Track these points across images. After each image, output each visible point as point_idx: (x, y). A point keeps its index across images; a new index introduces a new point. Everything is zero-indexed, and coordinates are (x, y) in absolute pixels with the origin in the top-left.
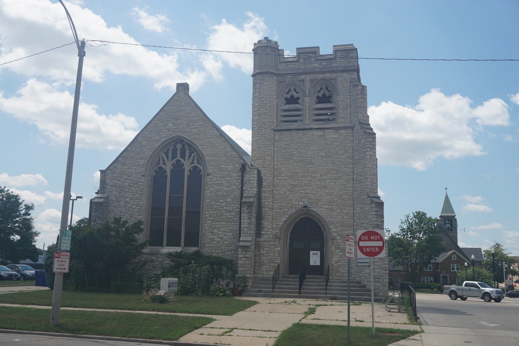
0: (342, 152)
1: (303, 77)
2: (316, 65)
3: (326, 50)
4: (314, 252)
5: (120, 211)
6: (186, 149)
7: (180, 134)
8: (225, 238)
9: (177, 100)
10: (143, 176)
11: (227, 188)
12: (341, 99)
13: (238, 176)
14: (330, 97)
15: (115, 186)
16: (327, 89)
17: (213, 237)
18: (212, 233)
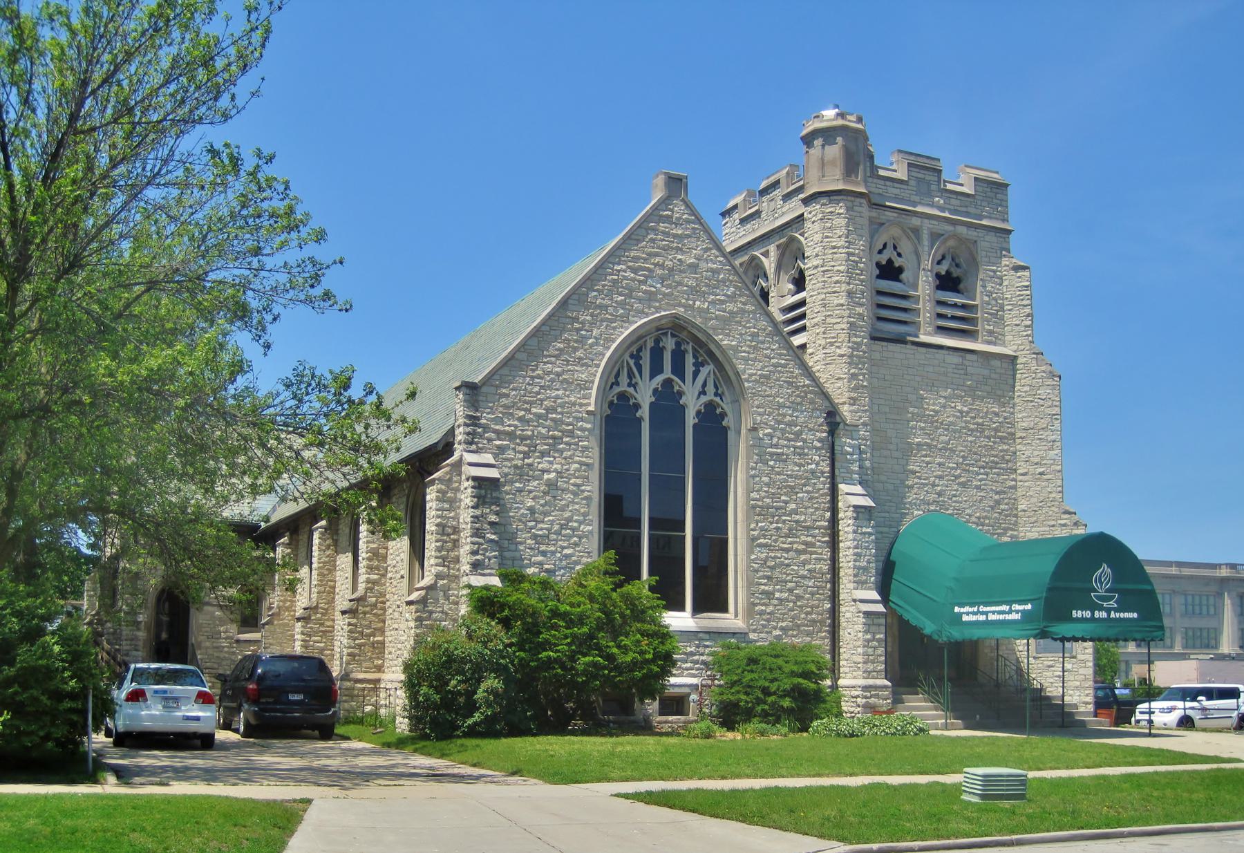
6: (685, 351)
16: (895, 248)
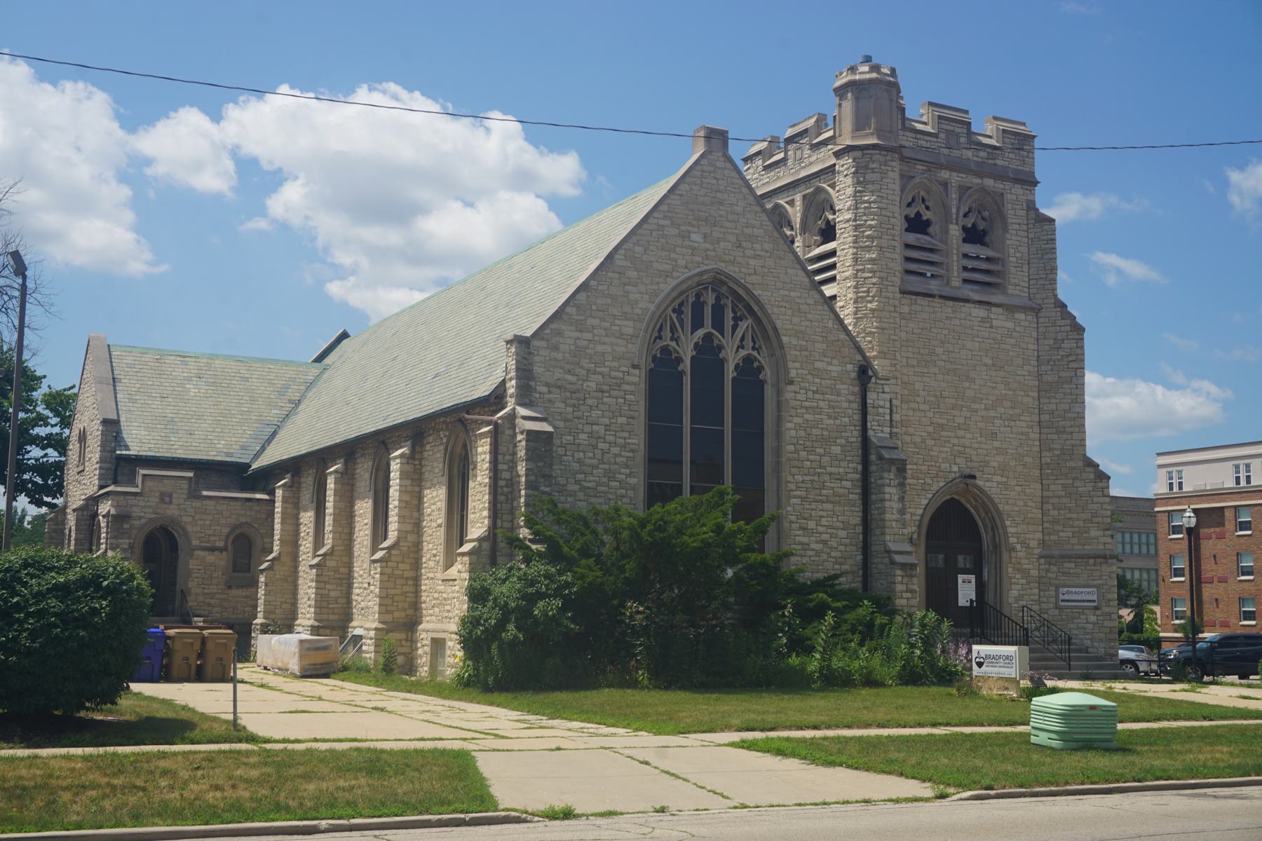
0: (1020, 361)
1: (945, 174)
2: (969, 154)
3: (987, 129)
4: (965, 576)
5: (579, 461)
7: (722, 266)
8: (834, 543)
9: (710, 172)
10: (634, 367)
11: (831, 422)
12: (1014, 243)
13: (853, 394)
14: (985, 232)
15: (560, 387)
17: (805, 540)
18: (804, 529)
